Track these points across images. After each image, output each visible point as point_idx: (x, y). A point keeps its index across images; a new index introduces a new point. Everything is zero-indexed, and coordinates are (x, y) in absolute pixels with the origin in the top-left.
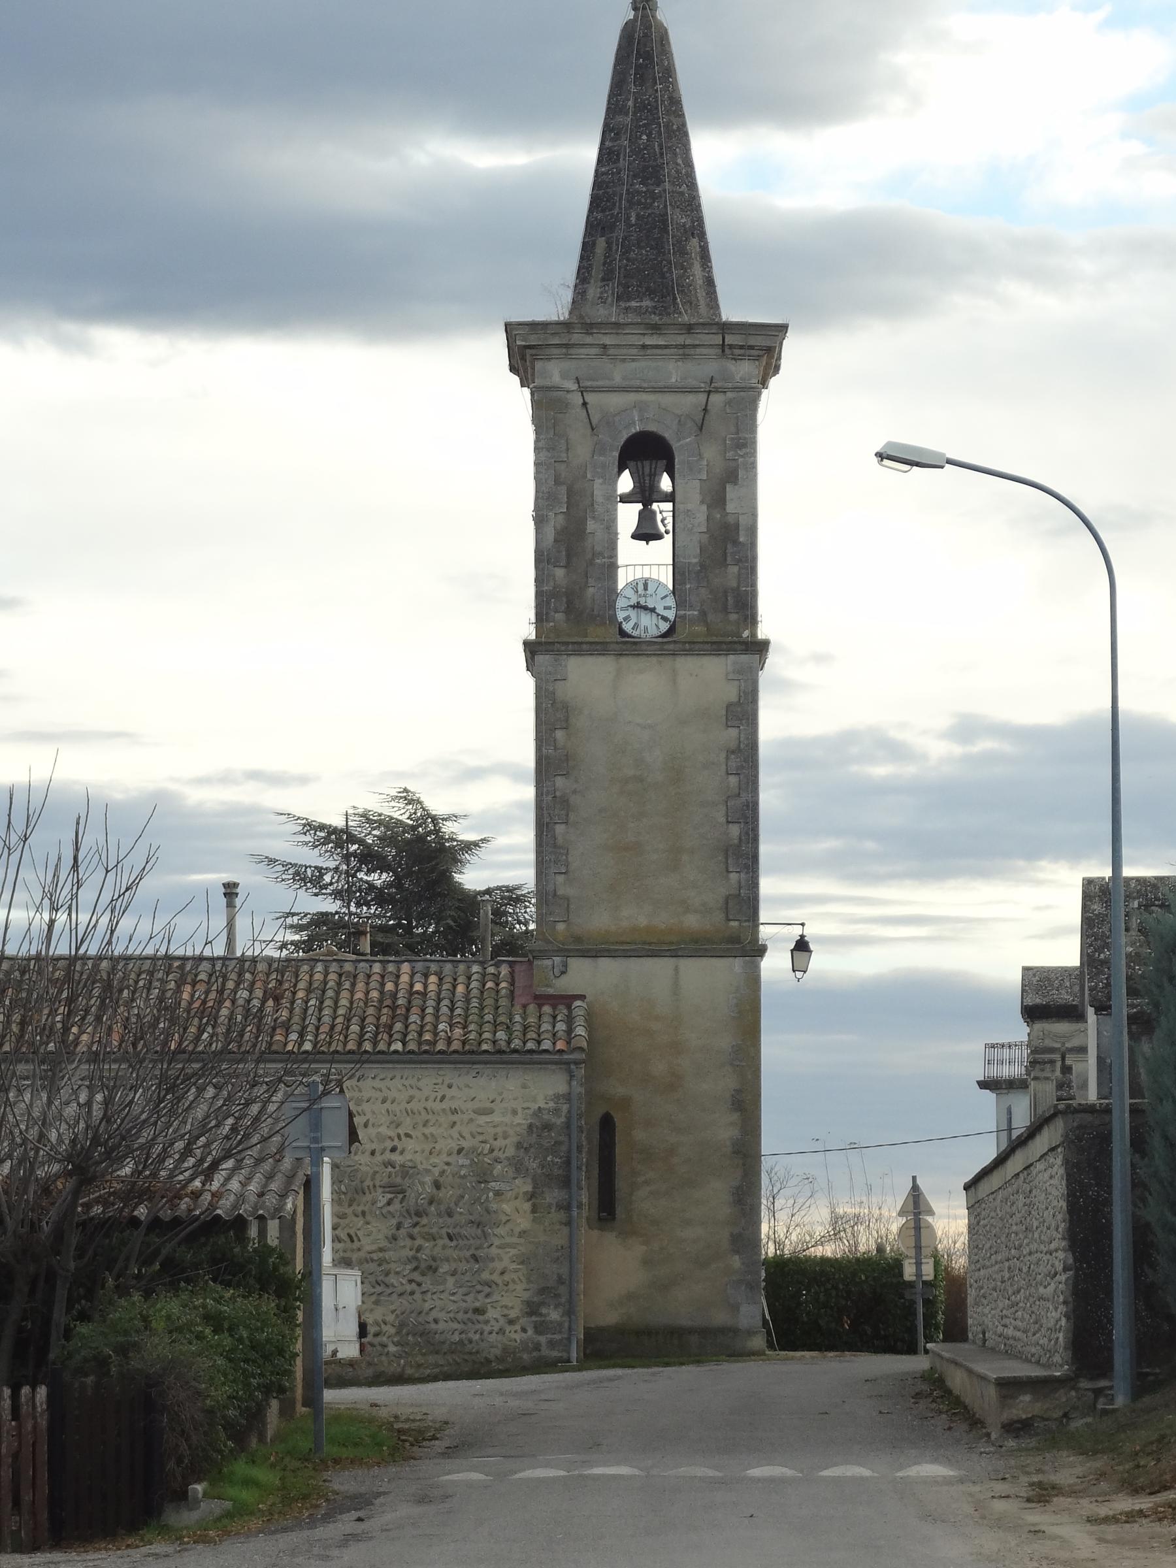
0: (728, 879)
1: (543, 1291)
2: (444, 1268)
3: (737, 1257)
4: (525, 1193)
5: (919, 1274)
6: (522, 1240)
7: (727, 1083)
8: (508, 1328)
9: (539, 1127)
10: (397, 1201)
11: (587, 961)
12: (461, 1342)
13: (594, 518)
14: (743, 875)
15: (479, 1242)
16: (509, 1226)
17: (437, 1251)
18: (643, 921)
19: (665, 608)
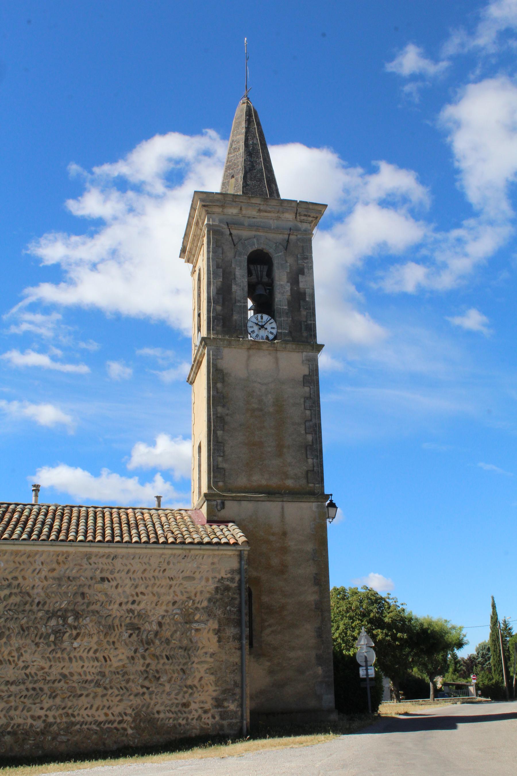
0: (307, 462)
1: (224, 692)
2: (164, 679)
3: (320, 668)
4: (214, 630)
5: (367, 674)
6: (211, 660)
7: (310, 570)
8: (204, 716)
9: (222, 589)
10: (134, 635)
11: (236, 502)
12: (175, 726)
13: (236, 284)
14: (315, 460)
15: (185, 661)
16: (204, 650)
17: (160, 666)
18: (264, 482)
19: (272, 328)
